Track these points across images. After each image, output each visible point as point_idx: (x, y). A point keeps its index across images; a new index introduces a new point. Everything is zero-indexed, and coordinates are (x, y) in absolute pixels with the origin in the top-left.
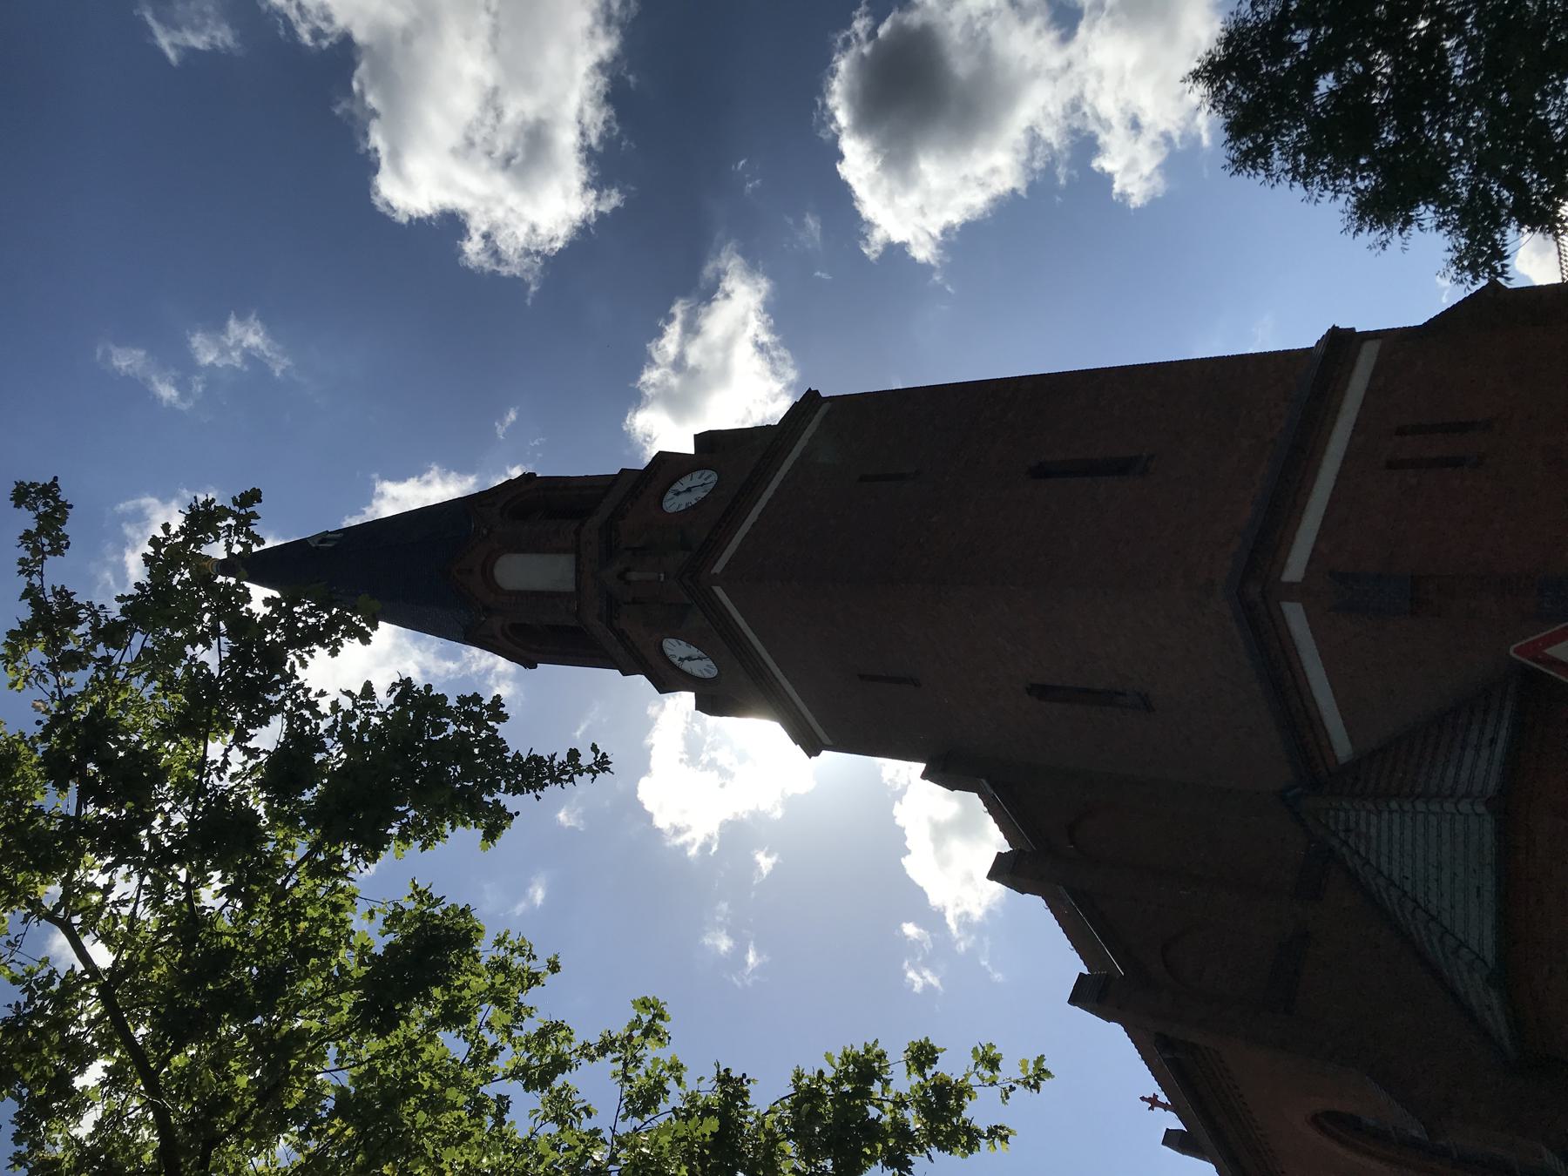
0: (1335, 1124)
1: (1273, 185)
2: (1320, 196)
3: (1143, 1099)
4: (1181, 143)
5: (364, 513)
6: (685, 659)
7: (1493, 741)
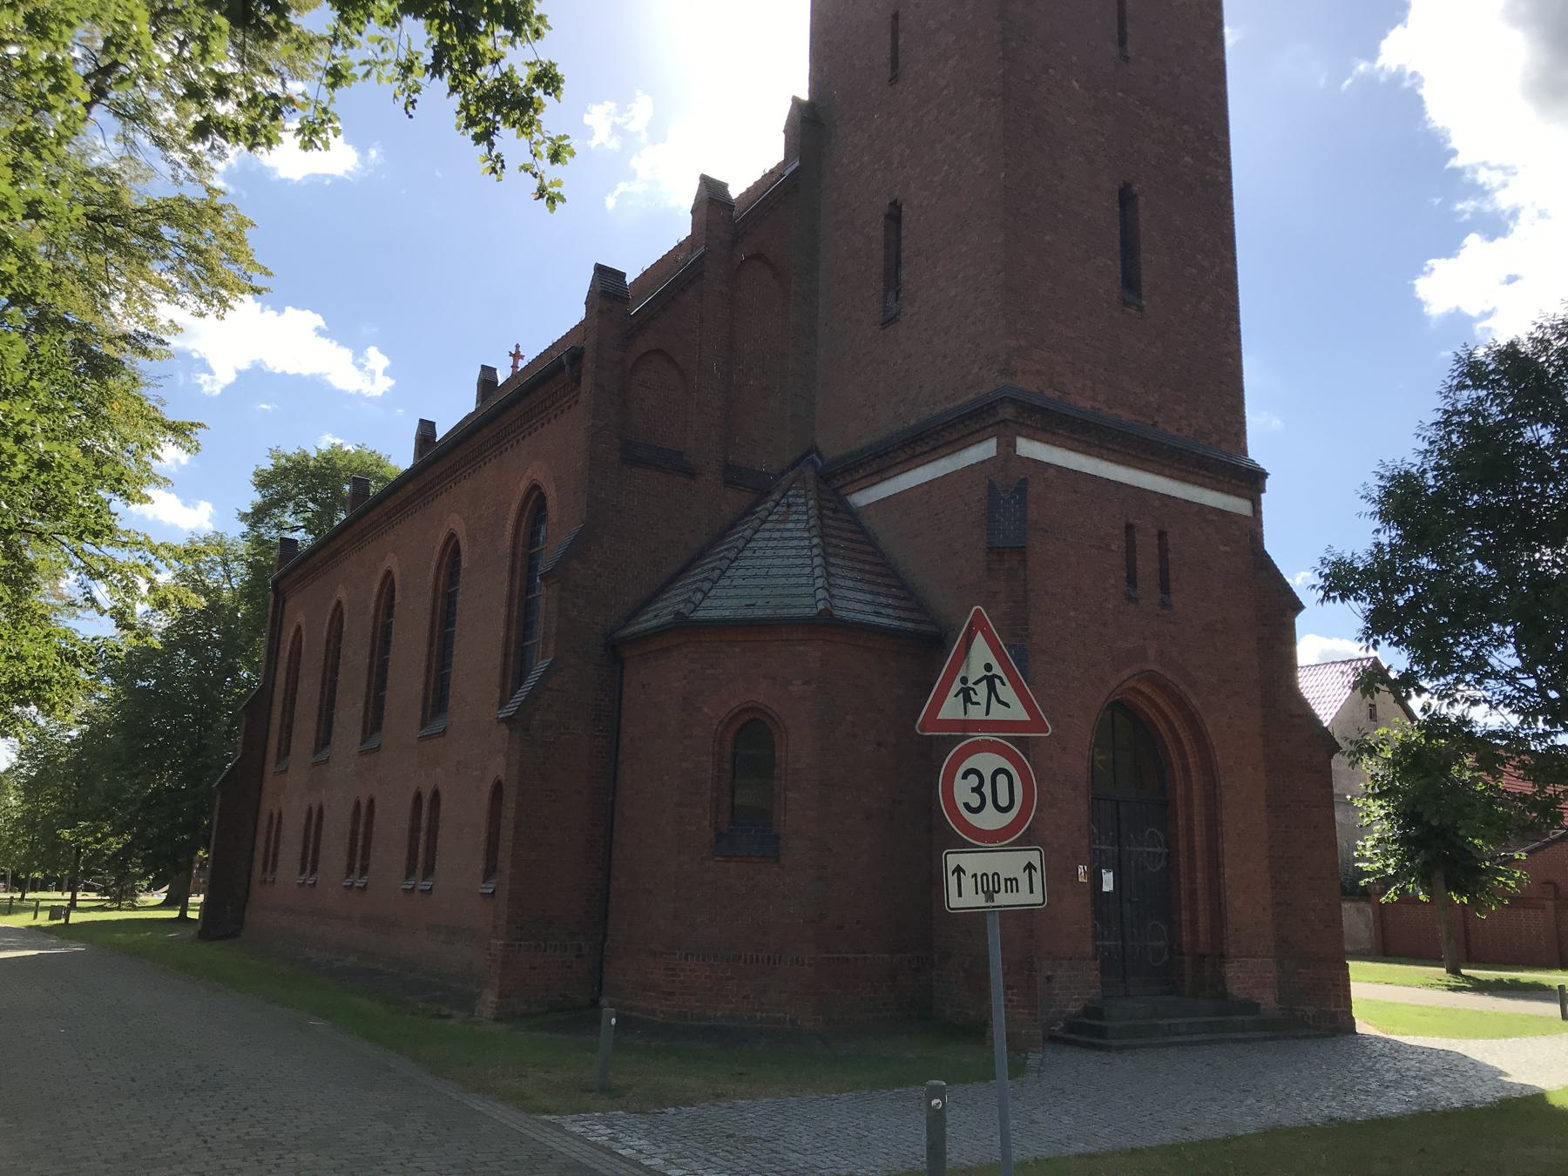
0: (535, 505)
1: (1441, 393)
2: (1424, 438)
3: (517, 346)
4: (1483, 329)
7: (878, 614)
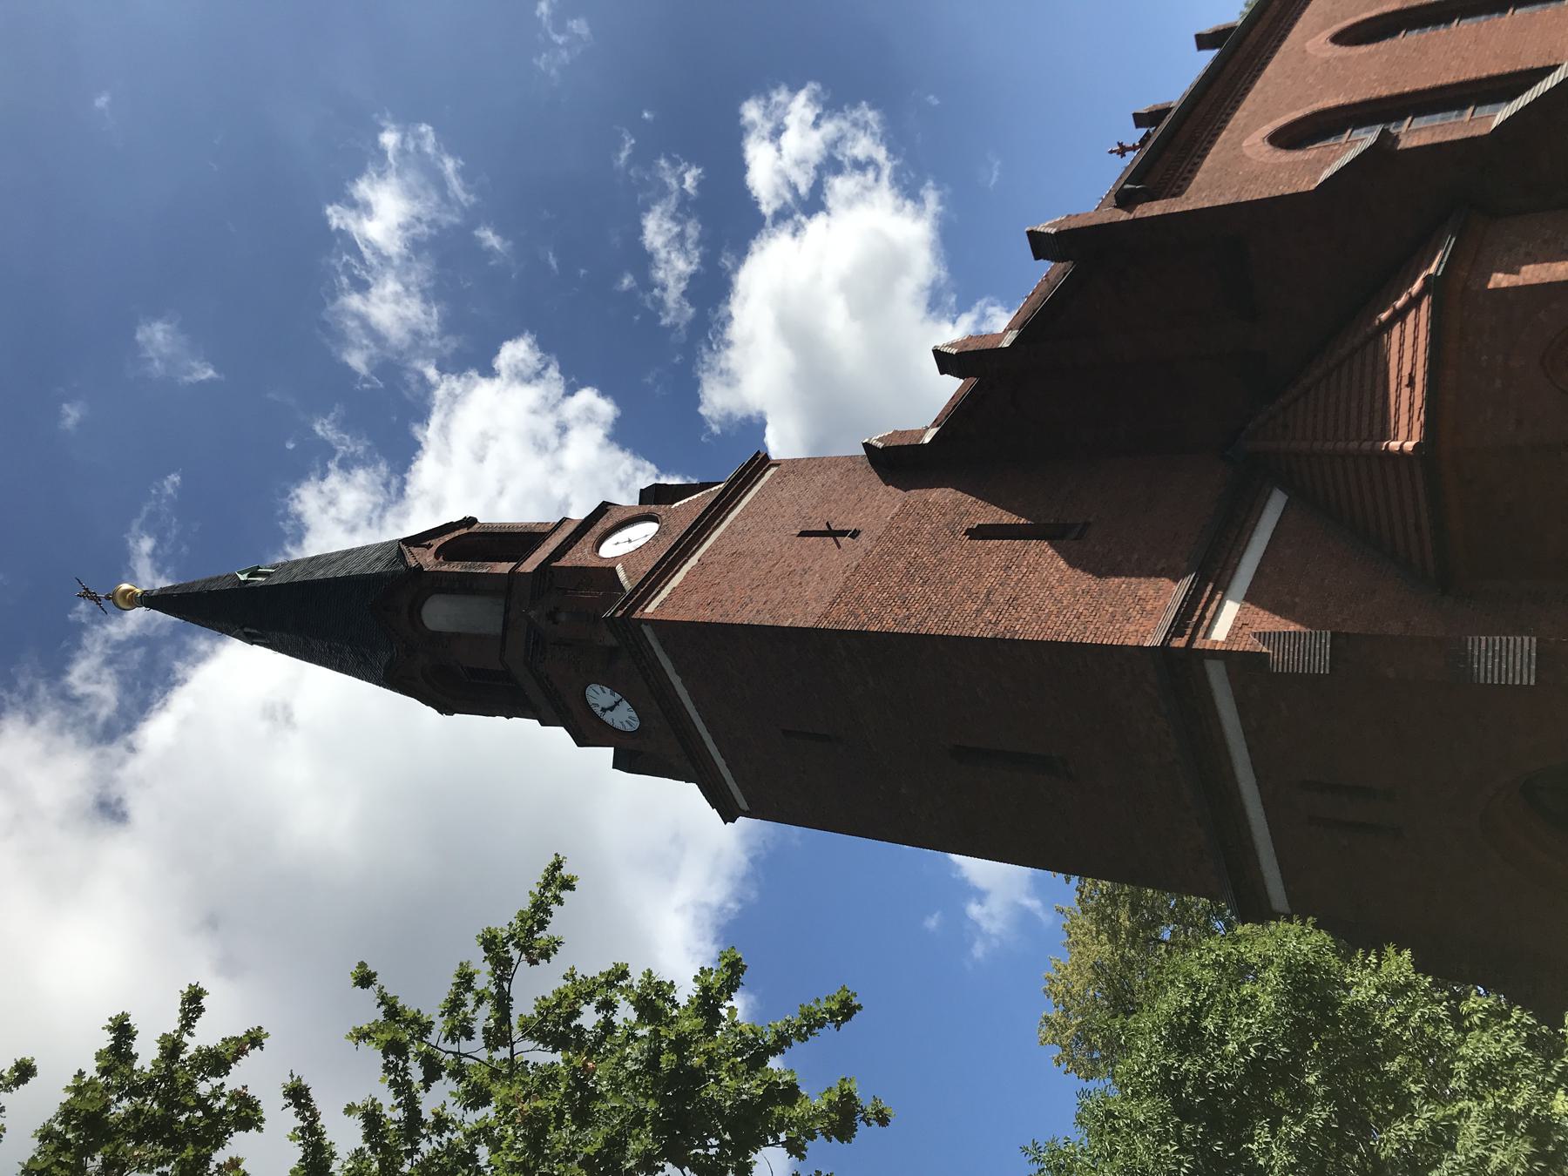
5: (678, 260)
6: (608, 709)
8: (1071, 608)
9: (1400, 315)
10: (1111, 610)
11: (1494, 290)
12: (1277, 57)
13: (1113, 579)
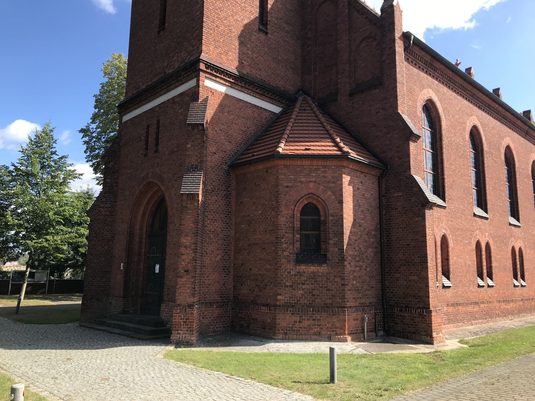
8: (222, 24)
9: (337, 145)
10: (221, 41)
11: (342, 177)
12: (471, 106)
13: (238, 42)
